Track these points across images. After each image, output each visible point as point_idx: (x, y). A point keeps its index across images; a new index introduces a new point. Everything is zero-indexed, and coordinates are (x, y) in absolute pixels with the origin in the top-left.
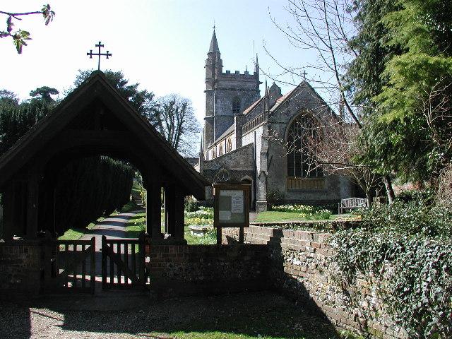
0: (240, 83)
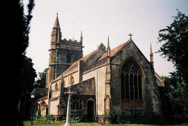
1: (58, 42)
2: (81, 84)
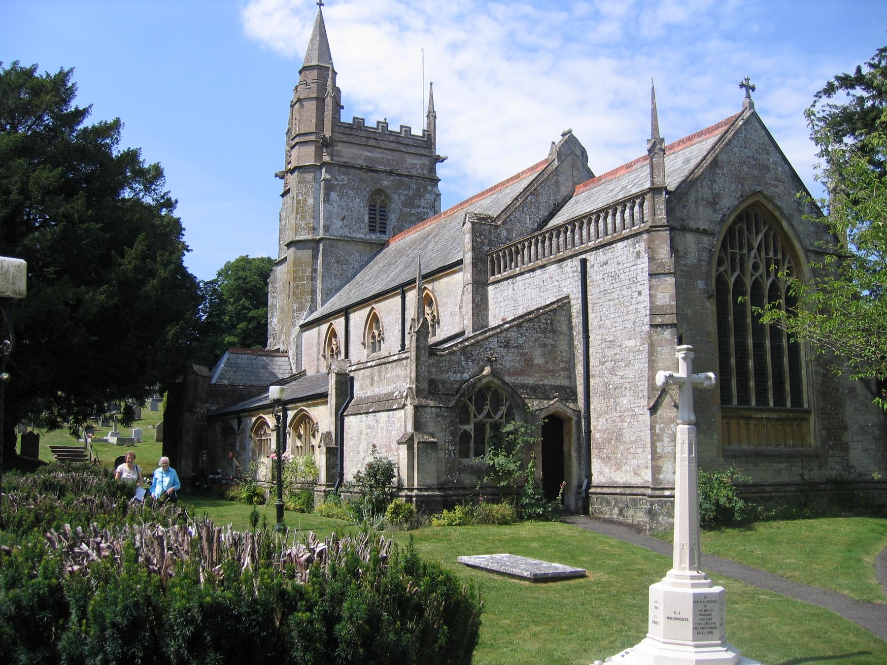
0: (390, 156)
1: (328, 134)
2: (507, 330)
